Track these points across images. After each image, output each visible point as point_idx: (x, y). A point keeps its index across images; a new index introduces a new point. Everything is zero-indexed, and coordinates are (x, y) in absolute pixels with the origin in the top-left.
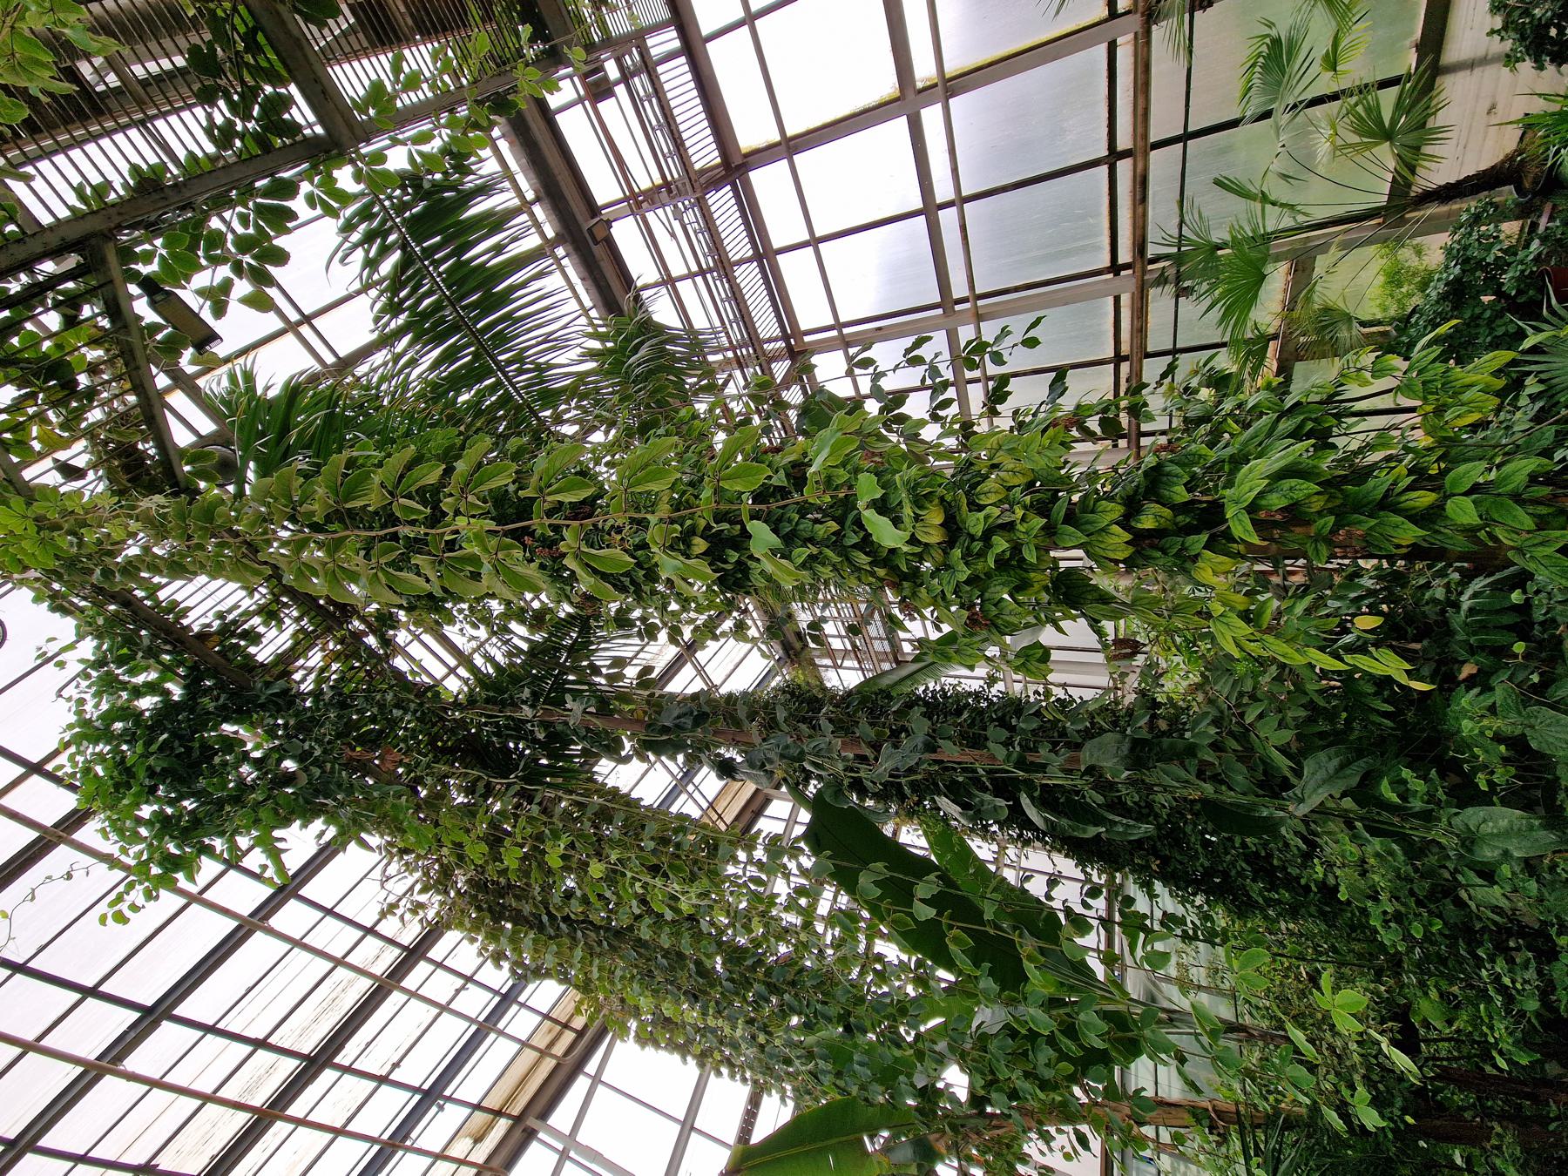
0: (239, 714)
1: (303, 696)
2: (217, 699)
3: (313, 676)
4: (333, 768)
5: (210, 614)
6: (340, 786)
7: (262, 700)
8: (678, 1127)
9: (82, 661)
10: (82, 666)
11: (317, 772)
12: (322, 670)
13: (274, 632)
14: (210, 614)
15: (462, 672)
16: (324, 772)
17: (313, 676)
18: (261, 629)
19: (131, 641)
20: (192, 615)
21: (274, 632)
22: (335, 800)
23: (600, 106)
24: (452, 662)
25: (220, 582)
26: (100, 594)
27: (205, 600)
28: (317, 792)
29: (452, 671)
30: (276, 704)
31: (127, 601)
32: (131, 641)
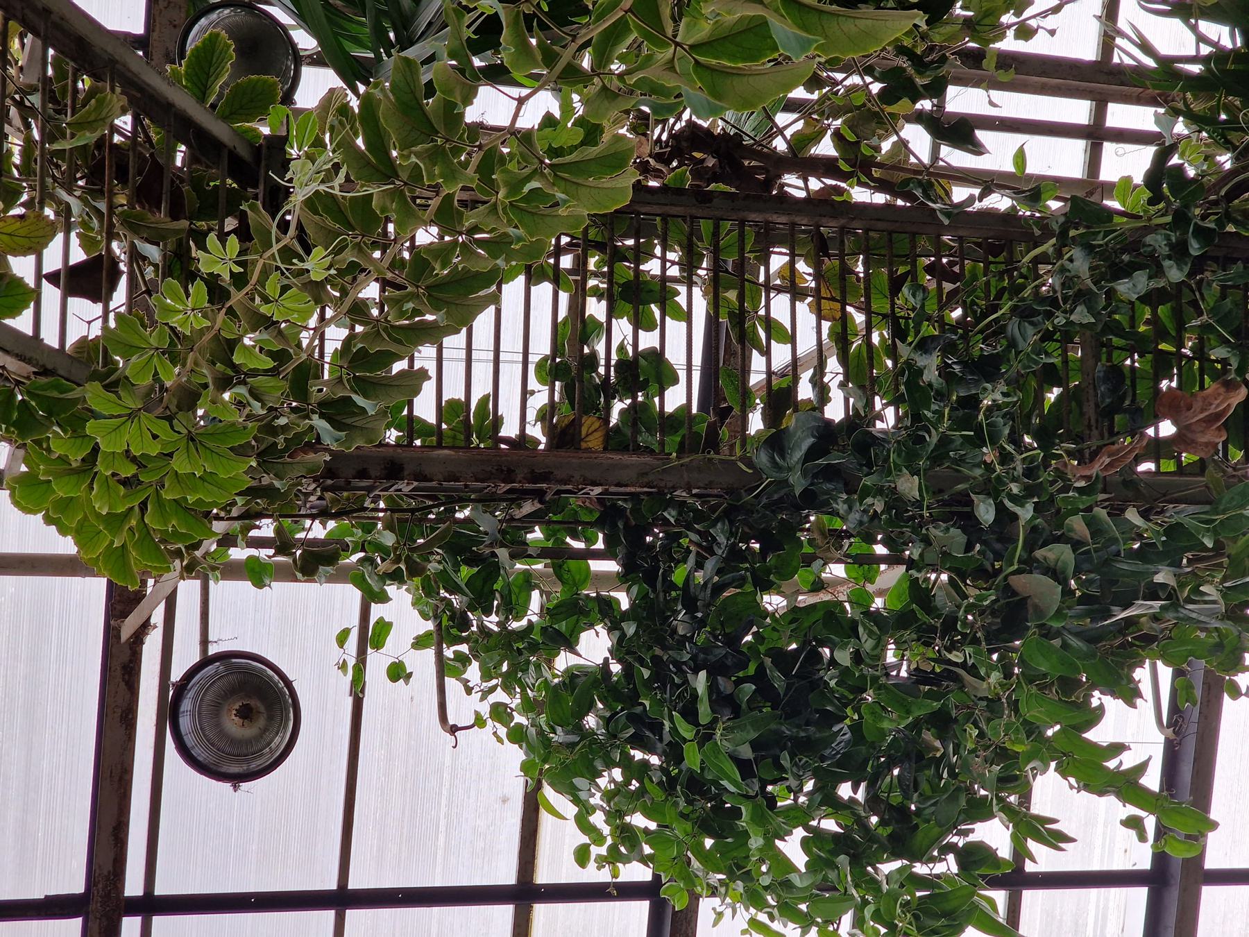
0: (779, 553)
1: (858, 422)
2: (708, 547)
3: (833, 364)
4: (1091, 523)
5: (533, 383)
6: (1147, 554)
7: (798, 483)
8: (332, 885)
9: (420, 643)
10: (430, 653)
11: (1060, 554)
12: (842, 337)
13: (675, 329)
14: (533, 383)
15: (1120, 115)
16: (1076, 545)
17: (833, 364)
18: (648, 340)
19: (461, 546)
20: (509, 409)
21: (675, 329)
22: (1153, 592)
23: (70, 300)
24: (1077, 111)
25: (483, 322)
26: (345, 482)
27: (495, 361)
28: (1096, 605)
29: (1096, 135)
30: (831, 473)
31: (393, 467)
32: (461, 546)
